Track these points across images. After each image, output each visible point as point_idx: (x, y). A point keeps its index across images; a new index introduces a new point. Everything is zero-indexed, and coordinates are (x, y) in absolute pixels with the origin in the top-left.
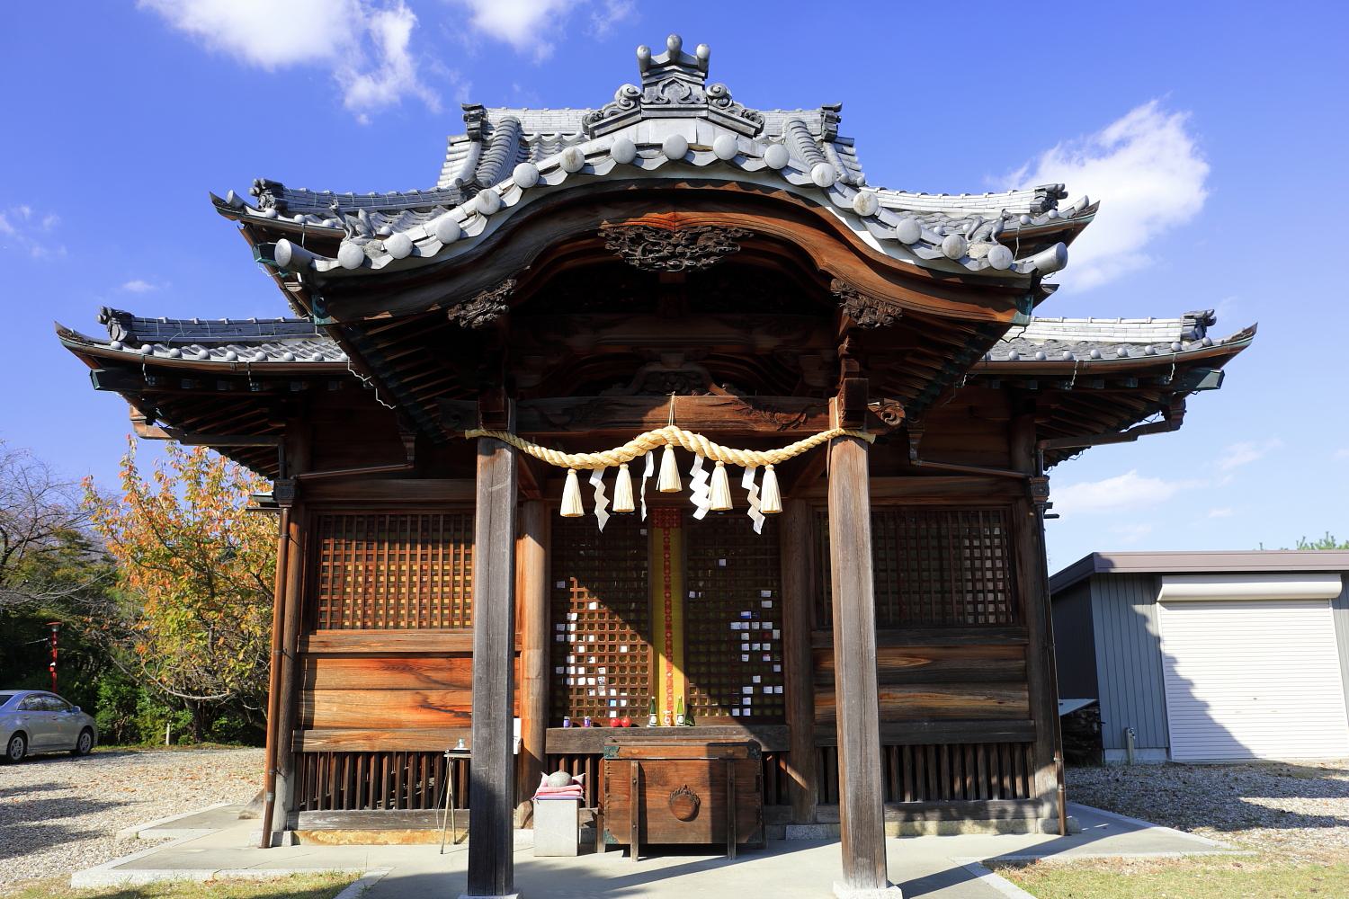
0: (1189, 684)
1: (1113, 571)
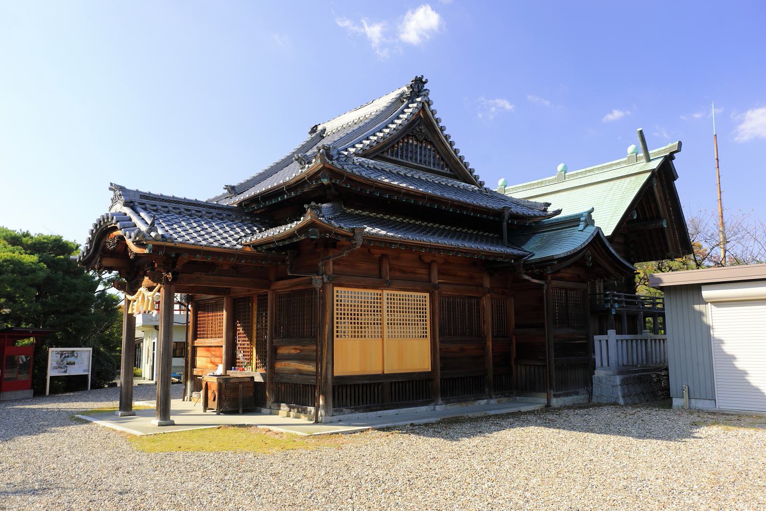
0: (733, 358)
1: (662, 285)
